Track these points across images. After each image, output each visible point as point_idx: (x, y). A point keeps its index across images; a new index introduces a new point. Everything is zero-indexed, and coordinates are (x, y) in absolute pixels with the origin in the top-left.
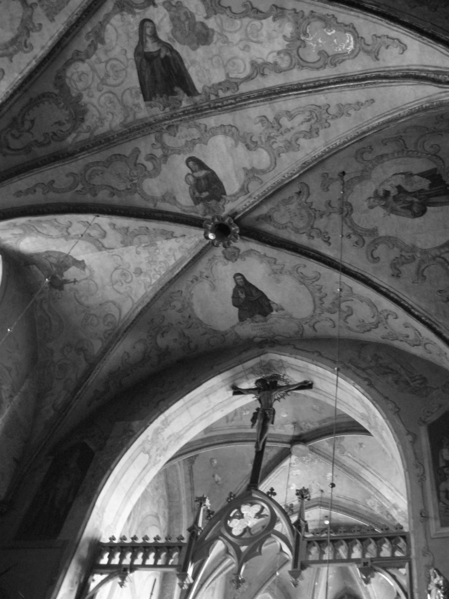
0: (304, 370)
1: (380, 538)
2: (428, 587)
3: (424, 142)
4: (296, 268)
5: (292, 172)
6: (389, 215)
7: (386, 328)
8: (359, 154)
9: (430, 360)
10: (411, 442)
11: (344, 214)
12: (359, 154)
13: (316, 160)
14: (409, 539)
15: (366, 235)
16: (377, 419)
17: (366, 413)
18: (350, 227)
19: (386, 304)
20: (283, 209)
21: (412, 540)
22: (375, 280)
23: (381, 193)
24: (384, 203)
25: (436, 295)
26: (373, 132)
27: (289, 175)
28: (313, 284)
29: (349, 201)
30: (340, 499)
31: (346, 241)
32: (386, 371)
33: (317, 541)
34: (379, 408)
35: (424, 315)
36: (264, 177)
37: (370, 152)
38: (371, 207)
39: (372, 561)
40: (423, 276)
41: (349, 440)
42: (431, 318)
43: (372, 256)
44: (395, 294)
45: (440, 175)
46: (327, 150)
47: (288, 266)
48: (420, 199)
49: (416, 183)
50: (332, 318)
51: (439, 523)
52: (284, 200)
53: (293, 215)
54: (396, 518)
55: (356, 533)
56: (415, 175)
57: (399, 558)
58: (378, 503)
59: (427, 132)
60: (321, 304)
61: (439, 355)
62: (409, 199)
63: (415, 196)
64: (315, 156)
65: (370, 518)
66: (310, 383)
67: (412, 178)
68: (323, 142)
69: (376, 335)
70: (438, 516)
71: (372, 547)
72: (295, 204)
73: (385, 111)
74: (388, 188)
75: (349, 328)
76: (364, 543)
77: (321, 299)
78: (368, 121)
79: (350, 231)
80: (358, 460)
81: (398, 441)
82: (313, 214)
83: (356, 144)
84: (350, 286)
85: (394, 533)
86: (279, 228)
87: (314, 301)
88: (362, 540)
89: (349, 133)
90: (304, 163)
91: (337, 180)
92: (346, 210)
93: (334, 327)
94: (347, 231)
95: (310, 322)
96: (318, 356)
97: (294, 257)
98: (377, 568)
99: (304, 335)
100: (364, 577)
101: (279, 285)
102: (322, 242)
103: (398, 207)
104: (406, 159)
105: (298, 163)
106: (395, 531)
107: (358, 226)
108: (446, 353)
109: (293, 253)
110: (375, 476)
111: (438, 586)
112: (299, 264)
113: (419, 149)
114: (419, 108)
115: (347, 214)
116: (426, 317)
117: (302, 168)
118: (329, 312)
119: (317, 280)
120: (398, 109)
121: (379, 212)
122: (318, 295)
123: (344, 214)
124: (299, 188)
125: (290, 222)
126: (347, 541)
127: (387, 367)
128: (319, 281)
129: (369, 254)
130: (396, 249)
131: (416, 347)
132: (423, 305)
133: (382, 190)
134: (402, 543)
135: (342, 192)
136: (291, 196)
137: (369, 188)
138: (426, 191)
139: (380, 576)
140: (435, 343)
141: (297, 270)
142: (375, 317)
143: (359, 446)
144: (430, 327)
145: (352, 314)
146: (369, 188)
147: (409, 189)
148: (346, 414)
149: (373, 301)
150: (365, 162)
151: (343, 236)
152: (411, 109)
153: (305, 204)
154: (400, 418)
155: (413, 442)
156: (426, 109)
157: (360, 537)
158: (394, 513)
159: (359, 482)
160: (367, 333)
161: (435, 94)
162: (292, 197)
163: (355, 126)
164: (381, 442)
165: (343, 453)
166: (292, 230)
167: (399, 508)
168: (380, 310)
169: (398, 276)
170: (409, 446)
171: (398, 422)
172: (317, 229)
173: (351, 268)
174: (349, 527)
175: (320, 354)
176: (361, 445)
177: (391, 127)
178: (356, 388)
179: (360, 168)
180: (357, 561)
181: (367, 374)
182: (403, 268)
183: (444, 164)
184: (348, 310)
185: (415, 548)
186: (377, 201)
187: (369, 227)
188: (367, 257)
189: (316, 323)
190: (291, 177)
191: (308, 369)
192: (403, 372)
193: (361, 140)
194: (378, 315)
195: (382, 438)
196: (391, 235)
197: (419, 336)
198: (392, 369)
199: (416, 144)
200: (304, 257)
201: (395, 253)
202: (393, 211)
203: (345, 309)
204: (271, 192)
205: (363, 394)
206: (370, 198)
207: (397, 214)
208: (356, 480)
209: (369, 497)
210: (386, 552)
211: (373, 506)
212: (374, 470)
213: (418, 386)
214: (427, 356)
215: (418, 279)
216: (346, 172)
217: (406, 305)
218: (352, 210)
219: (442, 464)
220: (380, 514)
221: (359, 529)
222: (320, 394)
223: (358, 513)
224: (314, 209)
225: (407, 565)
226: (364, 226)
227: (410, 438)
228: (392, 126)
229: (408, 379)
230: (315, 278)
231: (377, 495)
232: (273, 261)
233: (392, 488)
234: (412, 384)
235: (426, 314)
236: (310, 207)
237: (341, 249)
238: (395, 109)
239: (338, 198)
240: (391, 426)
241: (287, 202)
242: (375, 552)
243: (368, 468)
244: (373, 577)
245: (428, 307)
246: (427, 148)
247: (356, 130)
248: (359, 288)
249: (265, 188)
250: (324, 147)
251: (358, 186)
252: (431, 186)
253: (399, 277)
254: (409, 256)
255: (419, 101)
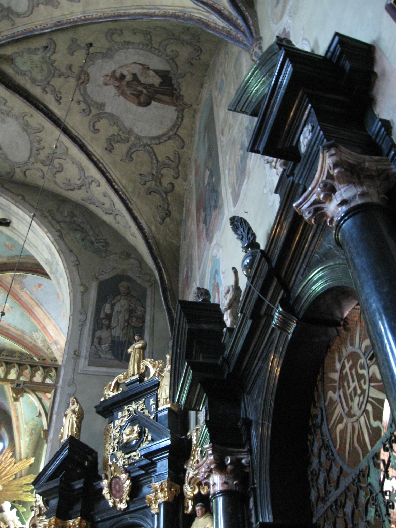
0: (5, 208)
1: (36, 366)
2: (65, 411)
3: (167, 45)
4: (24, 115)
5: (45, 25)
6: (119, 96)
7: (87, 192)
8: (110, 34)
9: (117, 229)
10: (82, 292)
11: (81, 81)
12: (110, 34)
13: (70, 23)
14: (60, 371)
15: (94, 106)
16: (58, 267)
17: (51, 260)
18: (82, 94)
19: (93, 172)
20: (26, 56)
21: (62, 372)
22: (90, 148)
23: (118, 75)
24: (117, 84)
25: (137, 176)
26: (127, 18)
27: (42, 28)
28: (35, 135)
29: (88, 71)
30: (10, 328)
31: (74, 105)
32: (78, 228)
33: (30, 365)
34: (63, 258)
35: (122, 190)
36: (18, 21)
37: (120, 35)
38: (106, 84)
39: (24, 384)
40: (131, 158)
41: (31, 279)
42: (127, 194)
43: (94, 126)
44: (103, 165)
45: (171, 77)
46: (83, 18)
47: (17, 111)
48: (148, 92)
49: (149, 77)
50: (43, 170)
51: (87, 362)
52: (29, 49)
53: (34, 66)
54: (54, 352)
55: (17, 359)
56: (151, 70)
57: (48, 385)
58: (42, 337)
59: (173, 37)
60: (37, 154)
61: (125, 227)
62: (140, 88)
63: (145, 88)
64: (70, 19)
65: (33, 348)
66: (8, 221)
67: (148, 71)
68: (81, 9)
69: (77, 196)
70: (88, 357)
71: (27, 372)
72: (39, 56)
73: (144, 4)
74: (125, 73)
75: (56, 183)
76: (21, 367)
77: (38, 150)
78: (126, 7)
79: (81, 98)
80: (34, 298)
81: (71, 288)
82: (53, 72)
83: (110, 23)
84: (67, 146)
85: (49, 364)
86: (18, 73)
87: (31, 150)
88: (20, 365)
89: (106, 10)
90: (59, 22)
91: (83, 48)
92: (83, 78)
93: (43, 178)
94: (78, 97)
95: (22, 167)
96: (22, 199)
97: (24, 104)
98: (27, 390)
99: (14, 178)
100: (15, 396)
101: (3, 125)
102: (53, 99)
103: (128, 92)
104: (148, 53)
105: (53, 19)
106: (50, 362)
107: (90, 97)
108: (130, 227)
109: (25, 101)
110: (45, 314)
111: (74, 411)
112: (27, 113)
113: (162, 50)
114: (172, 14)
115: (83, 82)
116: (123, 192)
117: (56, 25)
118: (42, 163)
119: (39, 132)
120: (156, 7)
121: (111, 90)
122: (36, 145)
123: (81, 81)
124: (47, 42)
125: (30, 71)
126: (7, 363)
127: (79, 226)
128: (41, 133)
129: (92, 124)
130: (115, 127)
131: (108, 215)
132: (124, 182)
133: (119, 72)
134: (53, 373)
135: (84, 61)
136: (37, 47)
137: (109, 66)
138: (155, 88)
139: (29, 398)
140: (124, 216)
141: (24, 117)
142: (81, 180)
143: (38, 286)
144: (124, 201)
145: (62, 171)
146: (109, 66)
147: (142, 79)
148: (33, 256)
149: (83, 165)
150: (113, 42)
151: (72, 100)
152: (166, 12)
153: (48, 59)
154: (78, 270)
155: (83, 293)
156: (177, 17)
157: (18, 362)
158: (54, 348)
159: (30, 316)
160: (70, 192)
161: (189, 8)
162: (38, 49)
163: (114, 6)
164: (57, 286)
165: (22, 289)
166: (30, 79)
167: (59, 344)
168: (86, 175)
169: (110, 151)
170: (79, 295)
171: (75, 273)
172: (53, 86)
173: (73, 131)
174: (12, 353)
175: (24, 198)
176: (40, 285)
177: (144, 20)
178: (48, 236)
179: (107, 45)
180: (12, 382)
181: (60, 226)
182: (116, 146)
183: (177, 69)
184: (59, 167)
185: (63, 379)
186: (112, 80)
187: (98, 100)
188: (89, 126)
189: (27, 169)
190: (43, 30)
191: (9, 208)
192: (91, 233)
193: (116, 21)
194: (84, 179)
195: (59, 283)
196: (115, 114)
197: (113, 206)
198: (82, 228)
199: (160, 43)
200: (33, 107)
201: (113, 130)
202: (123, 94)
203: (57, 165)
204: (20, 37)
205: (52, 243)
206: (107, 75)
207: (126, 98)
208: (28, 314)
209: (36, 331)
210: (38, 378)
211: (38, 339)
212: (45, 309)
213: (100, 247)
214: (115, 225)
215: (126, 159)
216: (94, 45)
217: (110, 177)
218: (88, 80)
219: (102, 316)
220: (42, 346)
221: (20, 356)
222: (14, 232)
223: (23, 342)
224: (55, 67)
225: (53, 391)
226: (94, 98)
227: (82, 289)
228: (145, 19)
229: (94, 239)
230: (38, 129)
231: (43, 330)
232: (4, 102)
233: (57, 327)
234: (96, 244)
235: (124, 190)
236: (52, 64)
237: (68, 111)
238: (152, 6)
239: (80, 65)
240: (68, 275)
241: (33, 51)
242: (29, 376)
243: (41, 306)
244: (22, 396)
245: (127, 185)
246: (168, 51)
247: (114, 10)
248: (74, 151)
249: (15, 31)
250: (82, 14)
251: (100, 61)
252: (161, 84)
253: (112, 152)
254: (125, 137)
255: (174, 8)
